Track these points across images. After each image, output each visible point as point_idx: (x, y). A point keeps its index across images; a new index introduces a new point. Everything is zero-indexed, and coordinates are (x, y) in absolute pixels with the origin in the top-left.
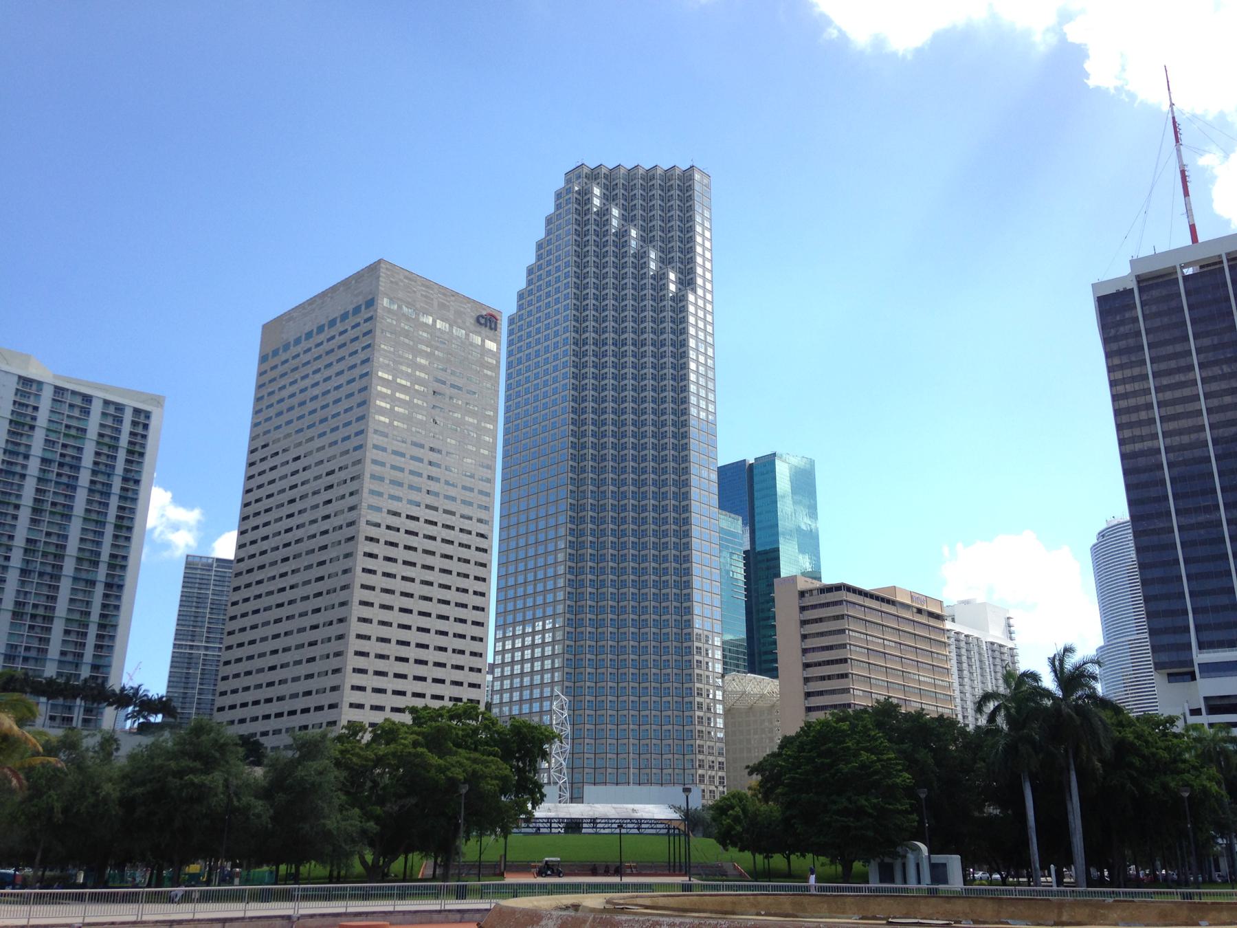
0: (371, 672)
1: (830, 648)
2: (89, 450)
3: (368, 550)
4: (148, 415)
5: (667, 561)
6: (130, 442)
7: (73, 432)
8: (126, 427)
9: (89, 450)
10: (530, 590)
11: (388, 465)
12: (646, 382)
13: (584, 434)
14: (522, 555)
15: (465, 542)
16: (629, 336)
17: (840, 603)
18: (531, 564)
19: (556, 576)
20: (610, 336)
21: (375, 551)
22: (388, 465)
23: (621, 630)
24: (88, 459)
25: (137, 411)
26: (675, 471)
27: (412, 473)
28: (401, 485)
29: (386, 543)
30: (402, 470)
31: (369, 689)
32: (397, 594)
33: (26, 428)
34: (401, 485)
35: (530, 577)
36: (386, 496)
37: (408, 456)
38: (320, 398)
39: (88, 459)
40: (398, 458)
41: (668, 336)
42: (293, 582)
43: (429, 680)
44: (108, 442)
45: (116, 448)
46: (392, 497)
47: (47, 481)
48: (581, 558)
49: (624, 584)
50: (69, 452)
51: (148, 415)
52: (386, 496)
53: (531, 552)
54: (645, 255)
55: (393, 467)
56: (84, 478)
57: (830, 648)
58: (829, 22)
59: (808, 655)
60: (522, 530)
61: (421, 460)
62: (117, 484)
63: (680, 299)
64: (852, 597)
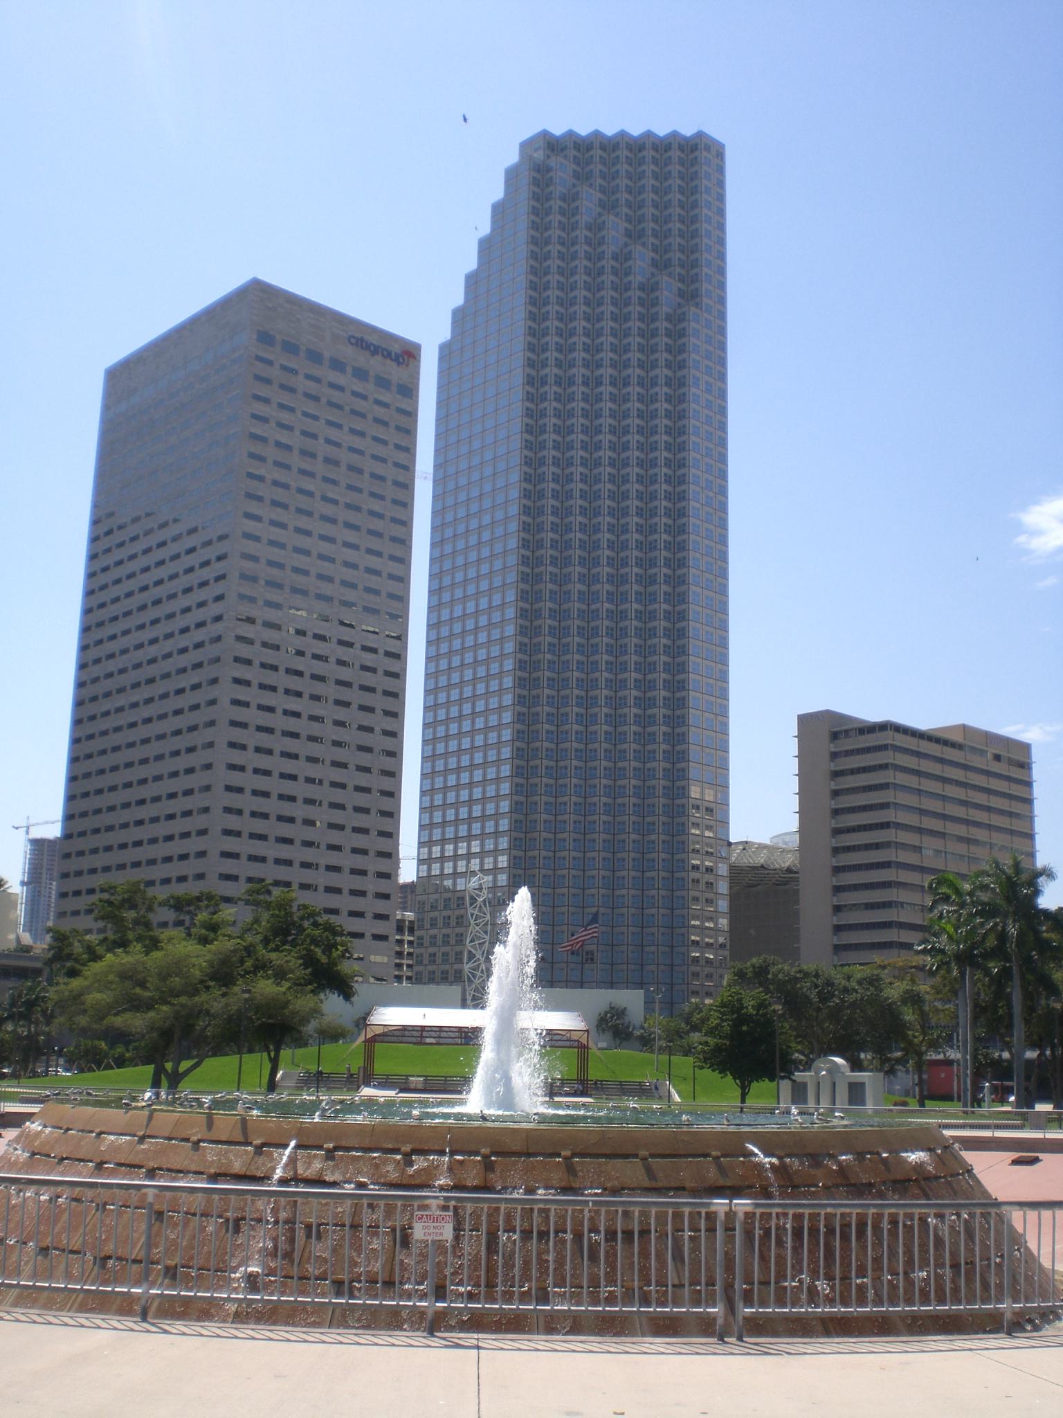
0: (245, 835)
1: (877, 846)
3: (237, 675)
5: (654, 723)
11: (263, 561)
12: (629, 437)
13: (541, 495)
15: (369, 664)
16: (607, 372)
17: (885, 786)
18: (468, 692)
19: (498, 779)
20: (579, 372)
21: (248, 677)
22: (263, 561)
23: (590, 764)
26: (667, 667)
27: (296, 570)
28: (280, 586)
30: (281, 566)
34: (280, 586)
35: (467, 709)
36: (260, 603)
37: (290, 548)
38: (130, 665)
40: (276, 550)
41: (663, 372)
46: (269, 604)
48: (537, 631)
49: (595, 649)
54: (655, 287)
55: (271, 563)
57: (877, 846)
59: (840, 779)
61: (307, 553)
63: (677, 319)
64: (901, 740)
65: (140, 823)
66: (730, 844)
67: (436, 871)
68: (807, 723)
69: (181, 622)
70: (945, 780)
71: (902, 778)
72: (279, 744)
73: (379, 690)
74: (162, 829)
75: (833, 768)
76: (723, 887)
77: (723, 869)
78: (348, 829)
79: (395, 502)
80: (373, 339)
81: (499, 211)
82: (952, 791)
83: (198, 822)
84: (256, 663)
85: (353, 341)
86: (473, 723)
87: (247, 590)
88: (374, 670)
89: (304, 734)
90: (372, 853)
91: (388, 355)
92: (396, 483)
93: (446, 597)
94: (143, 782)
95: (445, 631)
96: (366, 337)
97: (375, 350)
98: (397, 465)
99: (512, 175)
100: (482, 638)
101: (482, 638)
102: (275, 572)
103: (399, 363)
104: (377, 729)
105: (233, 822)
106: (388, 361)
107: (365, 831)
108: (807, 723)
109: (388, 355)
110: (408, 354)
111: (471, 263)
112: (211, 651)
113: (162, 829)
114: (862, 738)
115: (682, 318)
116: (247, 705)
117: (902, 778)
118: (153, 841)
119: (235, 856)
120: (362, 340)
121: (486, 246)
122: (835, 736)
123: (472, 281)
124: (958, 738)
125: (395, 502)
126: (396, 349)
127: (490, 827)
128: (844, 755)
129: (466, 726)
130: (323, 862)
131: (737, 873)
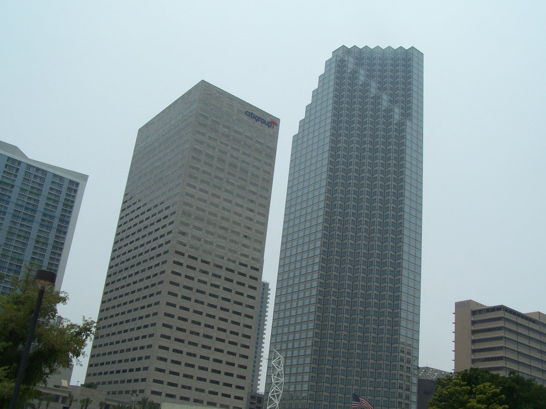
2: (43, 201)
3: (176, 260)
4: (77, 184)
6: (65, 199)
7: (35, 191)
8: (64, 190)
9: (43, 201)
10: (294, 304)
14: (291, 282)
15: (244, 262)
21: (181, 261)
24: (41, 207)
25: (71, 182)
29: (189, 256)
31: (171, 350)
32: (194, 290)
33: (10, 186)
36: (191, 227)
39: (41, 207)
40: (202, 203)
42: (135, 280)
43: (213, 349)
44: (53, 200)
45: (57, 202)
47: (18, 217)
50: (32, 202)
51: (77, 184)
52: (191, 227)
53: (297, 281)
54: (391, 110)
56: (38, 217)
58: (466, 371)
59: (476, 316)
60: (292, 267)
62: (56, 222)
63: (401, 125)
65: (126, 331)
66: (419, 368)
67: (292, 388)
68: (460, 306)
69: (154, 236)
70: (530, 338)
71: (509, 335)
72: (194, 295)
73: (248, 276)
74: (133, 334)
75: (472, 319)
76: (415, 389)
77: (415, 380)
78: (227, 342)
79: (263, 188)
80: (257, 114)
81: (322, 79)
82: (533, 344)
83: (150, 330)
84: (186, 255)
85: (247, 113)
86: (297, 303)
87: (185, 220)
88: (246, 266)
89: (208, 292)
90: (238, 355)
91: (263, 122)
92: (264, 179)
93: (289, 245)
94: (130, 311)
95: (287, 261)
96: (254, 113)
97: (257, 119)
98: (265, 171)
99: (328, 63)
100: (304, 263)
101: (304, 263)
102: (200, 213)
103: (269, 127)
104: (245, 294)
105: (167, 331)
106: (264, 125)
107: (235, 344)
108: (460, 306)
109: (263, 122)
110: (273, 123)
111: (309, 100)
112: (165, 248)
113: (133, 334)
114: (488, 314)
115: (403, 124)
116: (180, 274)
117: (509, 335)
118: (130, 340)
119: (167, 349)
120: (252, 114)
121: (316, 94)
122: (474, 313)
123: (309, 108)
124: (537, 318)
125: (263, 188)
126: (268, 119)
127: (302, 352)
128: (479, 322)
129: (294, 304)
130: (212, 357)
131: (421, 383)
